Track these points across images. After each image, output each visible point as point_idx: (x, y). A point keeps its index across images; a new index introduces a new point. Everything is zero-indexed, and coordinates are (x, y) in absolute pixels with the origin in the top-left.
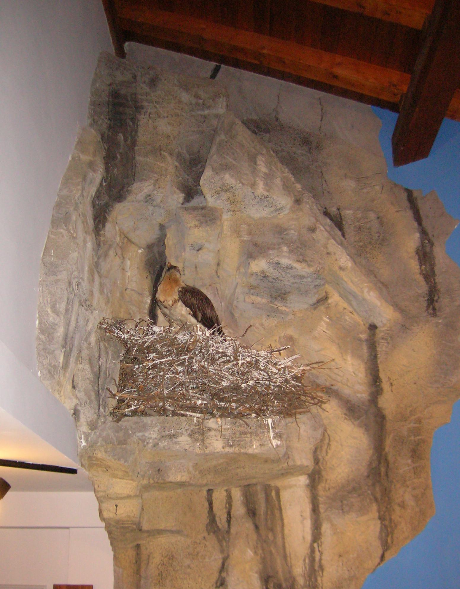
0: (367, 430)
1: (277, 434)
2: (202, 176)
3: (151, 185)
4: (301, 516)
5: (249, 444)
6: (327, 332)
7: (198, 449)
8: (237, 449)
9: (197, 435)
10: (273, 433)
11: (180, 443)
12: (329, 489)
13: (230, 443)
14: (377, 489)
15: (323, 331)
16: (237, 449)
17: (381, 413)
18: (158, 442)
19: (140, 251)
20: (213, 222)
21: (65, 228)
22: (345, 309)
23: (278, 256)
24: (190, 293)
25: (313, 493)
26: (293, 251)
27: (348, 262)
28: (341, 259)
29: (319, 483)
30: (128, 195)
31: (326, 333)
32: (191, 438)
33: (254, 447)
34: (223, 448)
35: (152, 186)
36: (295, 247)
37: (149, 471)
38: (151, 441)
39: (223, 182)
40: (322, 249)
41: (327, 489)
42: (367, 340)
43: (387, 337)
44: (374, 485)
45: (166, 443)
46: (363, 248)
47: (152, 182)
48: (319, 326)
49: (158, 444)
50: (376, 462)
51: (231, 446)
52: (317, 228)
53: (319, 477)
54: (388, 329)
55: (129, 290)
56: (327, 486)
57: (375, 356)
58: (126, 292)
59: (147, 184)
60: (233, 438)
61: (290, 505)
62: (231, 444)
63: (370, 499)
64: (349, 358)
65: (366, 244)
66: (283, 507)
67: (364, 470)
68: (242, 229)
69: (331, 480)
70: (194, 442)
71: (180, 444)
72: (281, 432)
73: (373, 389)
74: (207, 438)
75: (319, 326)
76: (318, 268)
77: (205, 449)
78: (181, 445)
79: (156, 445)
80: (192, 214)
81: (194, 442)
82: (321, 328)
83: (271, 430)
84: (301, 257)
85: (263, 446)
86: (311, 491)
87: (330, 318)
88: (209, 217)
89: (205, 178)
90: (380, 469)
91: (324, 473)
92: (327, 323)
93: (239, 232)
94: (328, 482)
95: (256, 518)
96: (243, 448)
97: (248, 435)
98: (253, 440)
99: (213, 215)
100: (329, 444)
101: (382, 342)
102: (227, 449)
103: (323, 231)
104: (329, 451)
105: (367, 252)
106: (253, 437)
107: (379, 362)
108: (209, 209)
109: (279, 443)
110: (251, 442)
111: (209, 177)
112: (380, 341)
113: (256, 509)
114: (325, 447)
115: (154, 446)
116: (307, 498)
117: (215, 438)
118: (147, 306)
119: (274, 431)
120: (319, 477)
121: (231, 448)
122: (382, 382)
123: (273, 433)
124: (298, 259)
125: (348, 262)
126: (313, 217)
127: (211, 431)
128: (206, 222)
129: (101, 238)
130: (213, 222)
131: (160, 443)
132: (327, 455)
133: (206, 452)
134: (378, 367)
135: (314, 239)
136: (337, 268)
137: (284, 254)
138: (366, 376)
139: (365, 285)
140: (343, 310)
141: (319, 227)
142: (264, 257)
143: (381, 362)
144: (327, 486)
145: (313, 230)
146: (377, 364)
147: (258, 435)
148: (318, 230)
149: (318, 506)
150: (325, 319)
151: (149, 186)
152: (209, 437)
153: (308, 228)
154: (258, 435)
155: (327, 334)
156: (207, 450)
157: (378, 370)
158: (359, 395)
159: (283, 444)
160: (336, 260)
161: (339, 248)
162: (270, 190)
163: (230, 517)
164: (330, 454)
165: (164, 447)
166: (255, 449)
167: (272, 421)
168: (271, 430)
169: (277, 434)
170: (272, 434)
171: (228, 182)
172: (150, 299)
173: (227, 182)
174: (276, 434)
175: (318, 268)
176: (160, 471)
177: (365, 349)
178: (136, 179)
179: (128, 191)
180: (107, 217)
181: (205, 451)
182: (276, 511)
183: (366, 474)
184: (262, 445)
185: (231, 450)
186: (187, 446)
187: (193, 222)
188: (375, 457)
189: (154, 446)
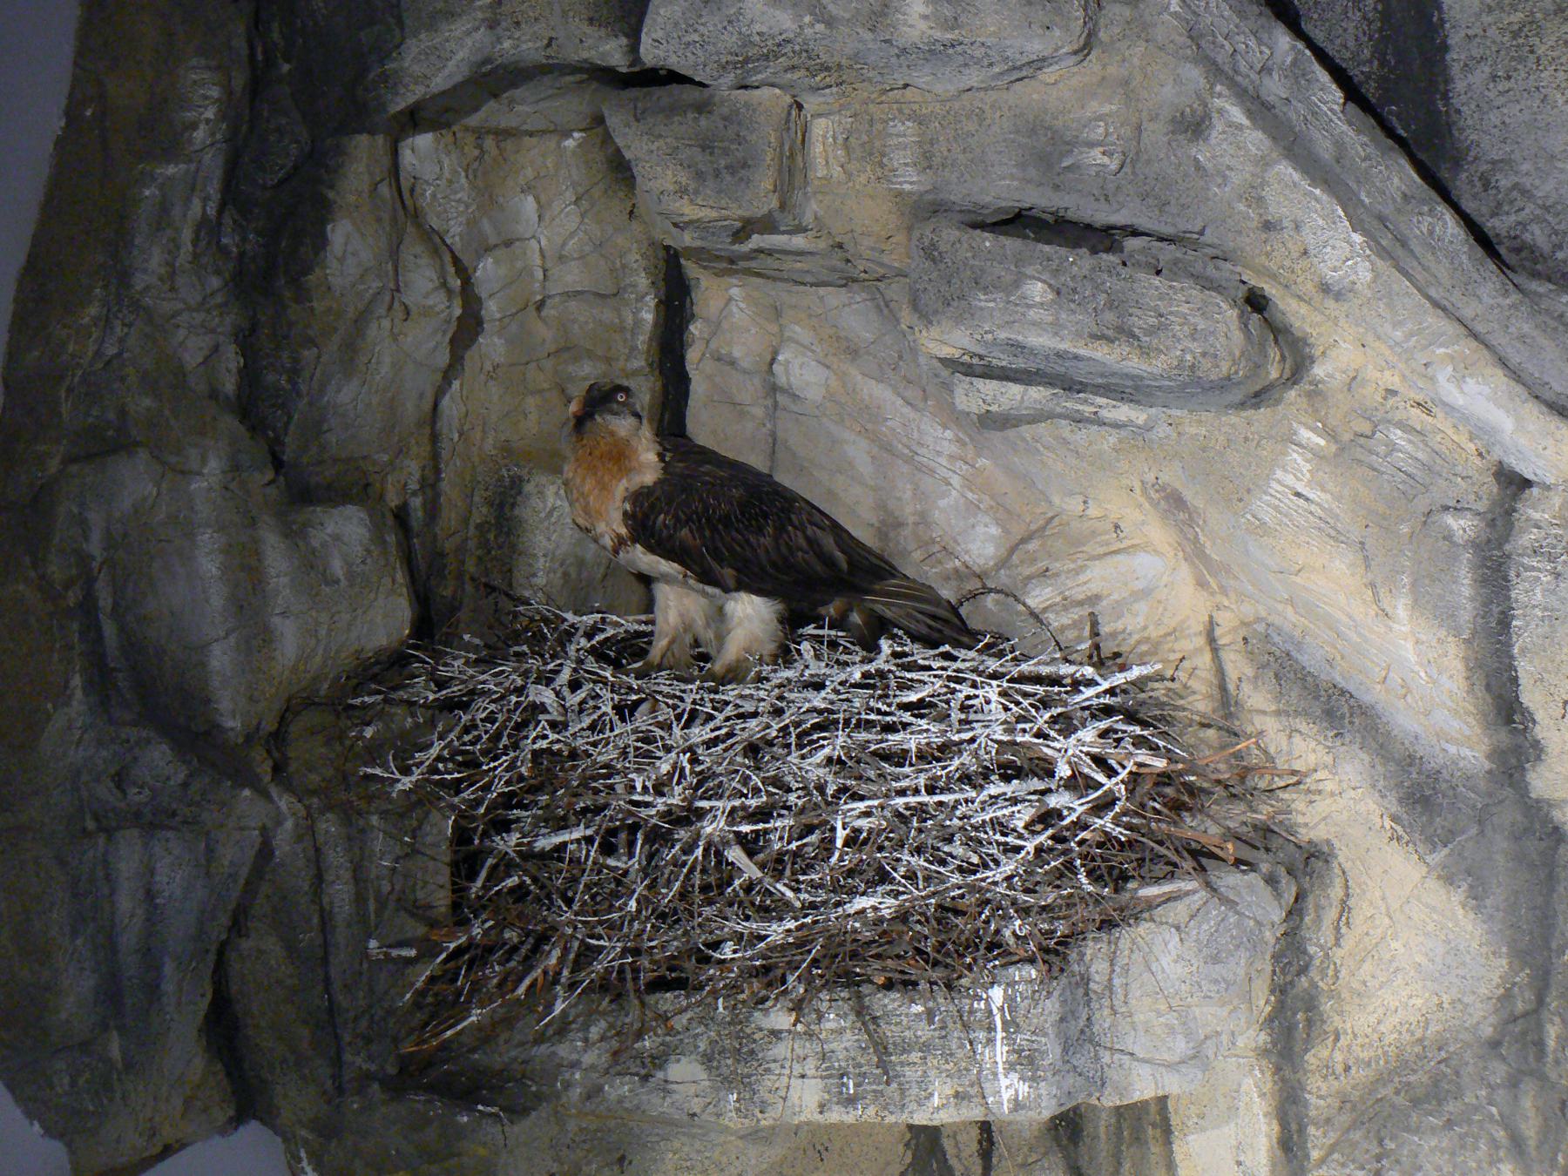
0: (1477, 896)
1: (1019, 1052)
2: (645, 30)
3: (478, 29)
4: (1239, 1163)
5: (915, 1091)
6: (1311, 496)
7: (734, 1114)
8: (871, 1111)
9: (729, 1062)
10: (1006, 1048)
11: (674, 1087)
12: (1347, 1069)
13: (848, 1089)
14: (1527, 1103)
15: (1298, 495)
16: (871, 1111)
17: (1547, 819)
18: (602, 1081)
19: (570, 143)
20: (741, 179)
21: (32, 574)
22: (1391, 393)
23: (1010, 323)
24: (667, 514)
25: (1283, 1080)
26: (1074, 291)
27: (1356, 263)
28: (1328, 249)
29: (1308, 1044)
30: (389, 96)
31: (1307, 499)
32: (709, 1069)
33: (936, 1101)
34: (822, 1108)
35: (482, 29)
36: (1085, 272)
37: (589, 1163)
38: (577, 1076)
39: (740, 33)
40: (1241, 207)
41: (1339, 1069)
42: (1475, 545)
43: (1554, 547)
44: (1513, 1083)
45: (626, 1088)
46: (1521, 41)
47: (480, 15)
48: (1279, 474)
49: (600, 1089)
50: (1529, 995)
51: (851, 1101)
52: (1215, 115)
53: (1309, 1023)
54: (1554, 521)
55: (557, 299)
56: (1338, 1057)
57: (1505, 622)
58: (543, 314)
59: (459, 27)
60: (860, 1066)
61: (1202, 1117)
62: (852, 1092)
63: (1494, 1144)
64: (1401, 608)
65: (1539, 15)
66: (1174, 1121)
67: (1482, 1018)
68: (895, 141)
69: (1355, 1036)
70: (718, 1090)
71: (674, 1091)
72: (1035, 1046)
73: (1503, 737)
74: (765, 1070)
75: (1279, 474)
76: (1189, 357)
77: (757, 1111)
78: (676, 1097)
79: (594, 1093)
80: (660, 136)
81: (718, 1090)
82: (1290, 480)
83: (1000, 1035)
84: (1110, 317)
85: (965, 1103)
86: (1278, 1069)
87: (1330, 434)
88: (726, 152)
89: (659, 34)
90: (1540, 1027)
91: (1327, 1006)
92: (1317, 455)
93: (883, 155)
94: (1343, 1042)
95: (1083, 1149)
96: (892, 1108)
97: (915, 1056)
98: (932, 1073)
99: (739, 139)
100: (1344, 907)
101: (1533, 569)
102: (836, 1115)
103: (1240, 127)
104: (1344, 930)
105: (1538, 59)
106: (932, 1062)
107: (1516, 651)
108: (725, 110)
109: (1024, 1089)
110: (923, 1082)
111: (676, 24)
112: (1526, 560)
113: (1081, 1116)
114: (1333, 913)
115: (589, 1097)
116: (1262, 1095)
117: (798, 1069)
118: (641, 338)
119: (1008, 1039)
120: (1309, 1023)
121: (850, 1109)
122: (1534, 722)
123: (1006, 1048)
124: (1095, 329)
125: (1356, 263)
126: (1196, 62)
127: (780, 1039)
128: (717, 174)
129: (315, 304)
130: (741, 179)
131: (606, 1088)
132: (1337, 944)
133: (763, 1123)
134: (1512, 668)
135: (1198, 166)
136: (1309, 285)
137: (1032, 314)
138: (1471, 690)
139: (1442, 351)
140: (1385, 398)
141: (1221, 111)
142: (958, 320)
143: (1523, 651)
144: (1338, 1057)
145: (1194, 126)
146: (1512, 657)
147: (951, 1055)
148: (1219, 125)
149: (1302, 1130)
150: (1305, 435)
151: (468, 33)
152: (772, 1066)
153: (1173, 120)
154: (951, 1055)
155: (1313, 508)
156: (767, 1115)
157: (1515, 681)
158: (1452, 749)
159: (1039, 1096)
160: (1305, 253)
161: (1317, 200)
162: (963, 19)
163: (991, 1142)
164: (1348, 942)
165: (620, 1102)
166: (938, 1109)
167: (1007, 998)
168: (1000, 1035)
169: (1019, 1052)
170: (1001, 1051)
171: (764, 29)
172: (652, 304)
173: (757, 27)
174: (1014, 1051)
175: (1189, 357)
176: (626, 1162)
177: (1464, 586)
178: (408, 22)
179: (384, 77)
180: (331, 195)
181: (758, 1121)
182: (1150, 1131)
183: (1487, 1031)
184: (963, 1099)
185: (850, 1117)
186: (696, 1100)
187: (669, 173)
188: (1523, 977)
189: (589, 1097)
